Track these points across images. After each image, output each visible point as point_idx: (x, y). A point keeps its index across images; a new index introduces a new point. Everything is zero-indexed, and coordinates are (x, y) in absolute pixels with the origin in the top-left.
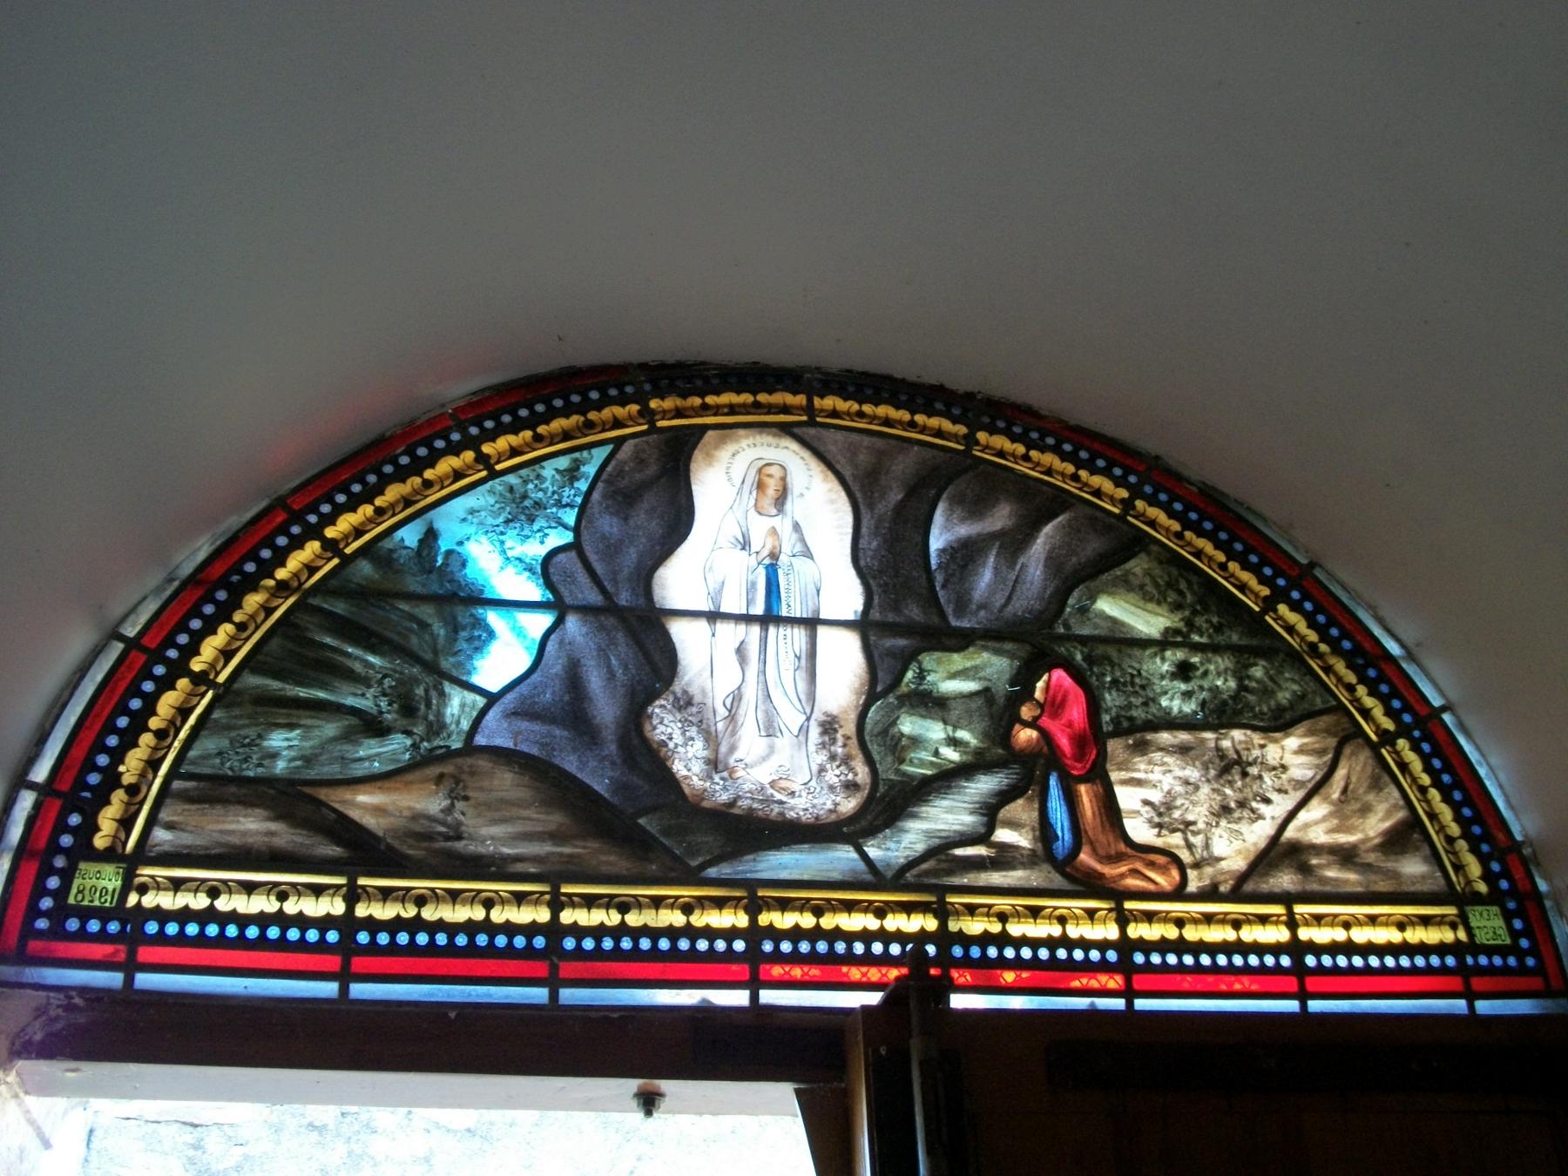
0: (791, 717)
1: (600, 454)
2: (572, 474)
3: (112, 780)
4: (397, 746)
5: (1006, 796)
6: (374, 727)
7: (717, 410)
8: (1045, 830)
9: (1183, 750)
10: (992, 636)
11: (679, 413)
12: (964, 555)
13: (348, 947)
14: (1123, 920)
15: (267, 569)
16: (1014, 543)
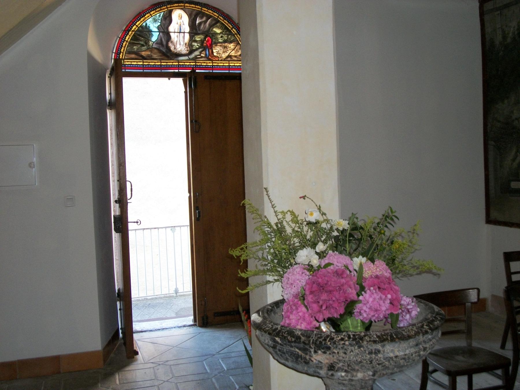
0: (182, 43)
1: (162, 13)
2: (160, 16)
3: (121, 52)
4: (145, 47)
5: (202, 51)
6: (143, 45)
7: (173, 7)
8: (206, 54)
9: (220, 46)
10: (202, 34)
11: (170, 7)
12: (200, 24)
13: (143, 67)
14: (213, 63)
15: (131, 29)
16: (205, 22)
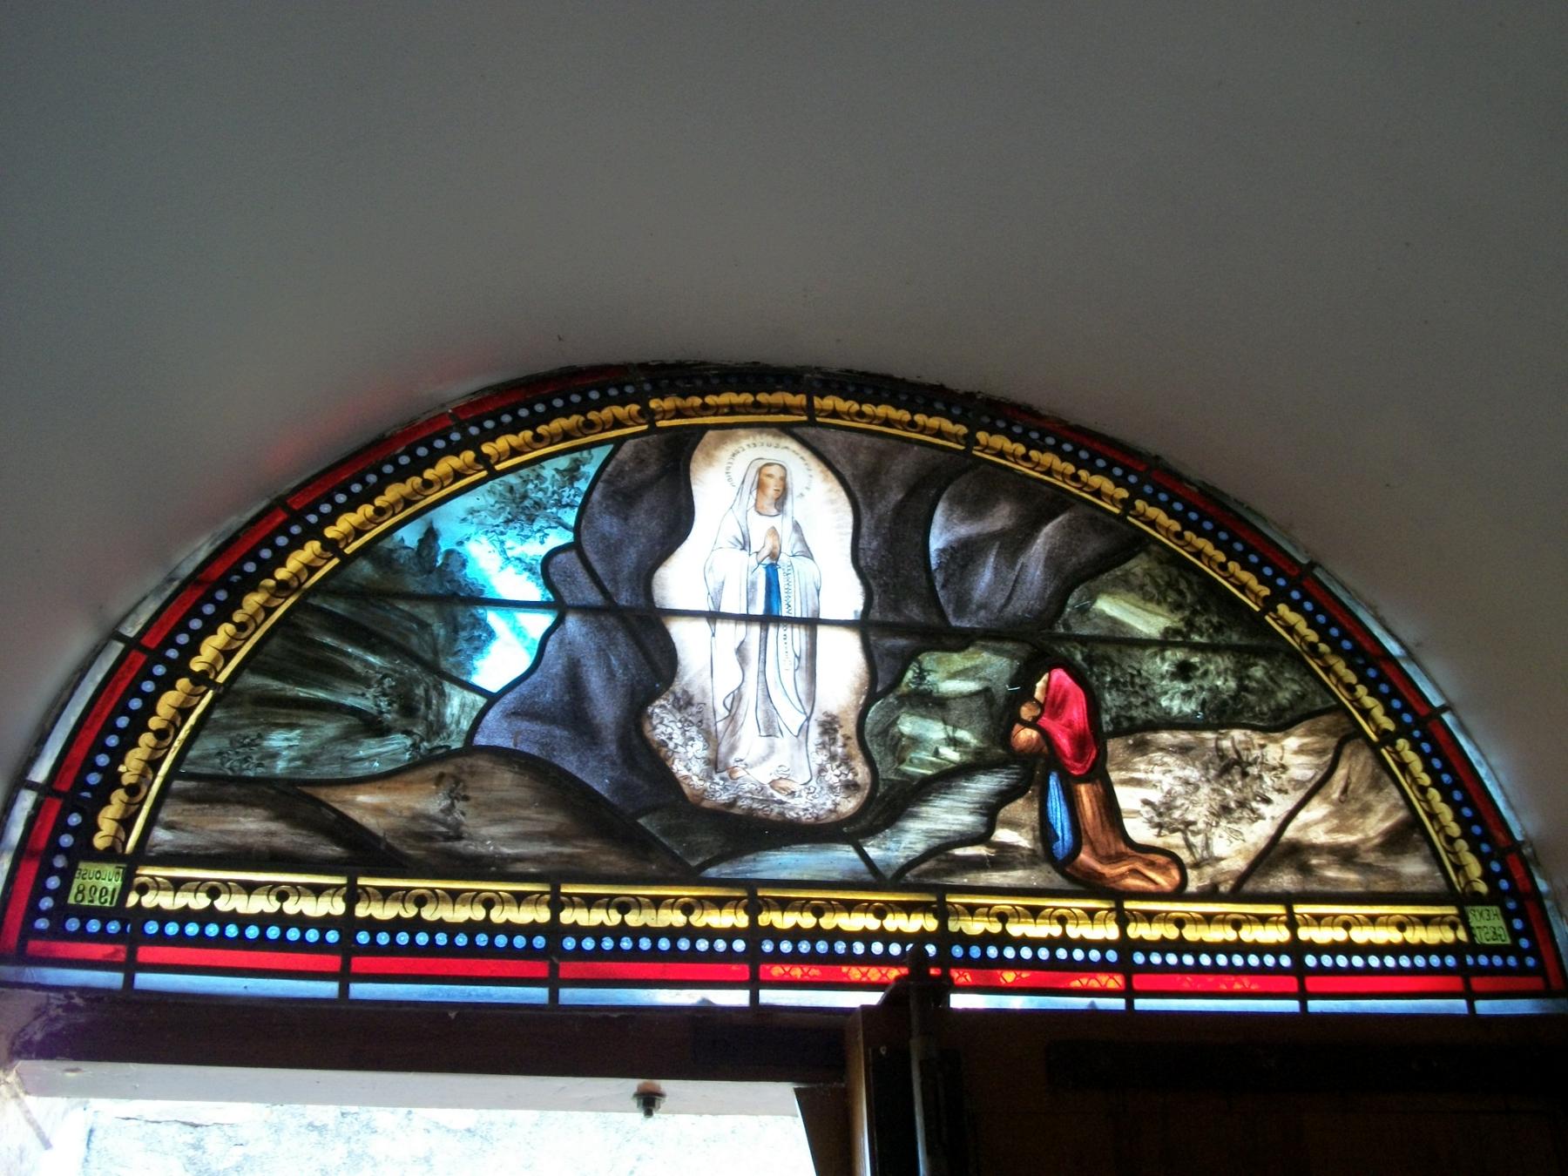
0: (791, 717)
1: (600, 454)
2: (572, 474)
3: (112, 780)
4: (397, 746)
5: (1006, 796)
6: (374, 727)
7: (717, 410)
8: (1045, 830)
9: (1183, 750)
10: (992, 636)
11: (679, 413)
12: (964, 555)
13: (348, 947)
14: (1123, 920)
15: (267, 569)
16: (1014, 543)
